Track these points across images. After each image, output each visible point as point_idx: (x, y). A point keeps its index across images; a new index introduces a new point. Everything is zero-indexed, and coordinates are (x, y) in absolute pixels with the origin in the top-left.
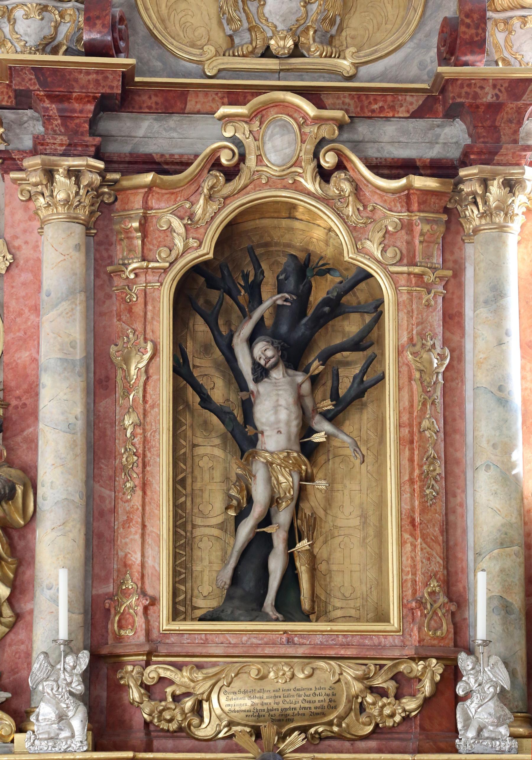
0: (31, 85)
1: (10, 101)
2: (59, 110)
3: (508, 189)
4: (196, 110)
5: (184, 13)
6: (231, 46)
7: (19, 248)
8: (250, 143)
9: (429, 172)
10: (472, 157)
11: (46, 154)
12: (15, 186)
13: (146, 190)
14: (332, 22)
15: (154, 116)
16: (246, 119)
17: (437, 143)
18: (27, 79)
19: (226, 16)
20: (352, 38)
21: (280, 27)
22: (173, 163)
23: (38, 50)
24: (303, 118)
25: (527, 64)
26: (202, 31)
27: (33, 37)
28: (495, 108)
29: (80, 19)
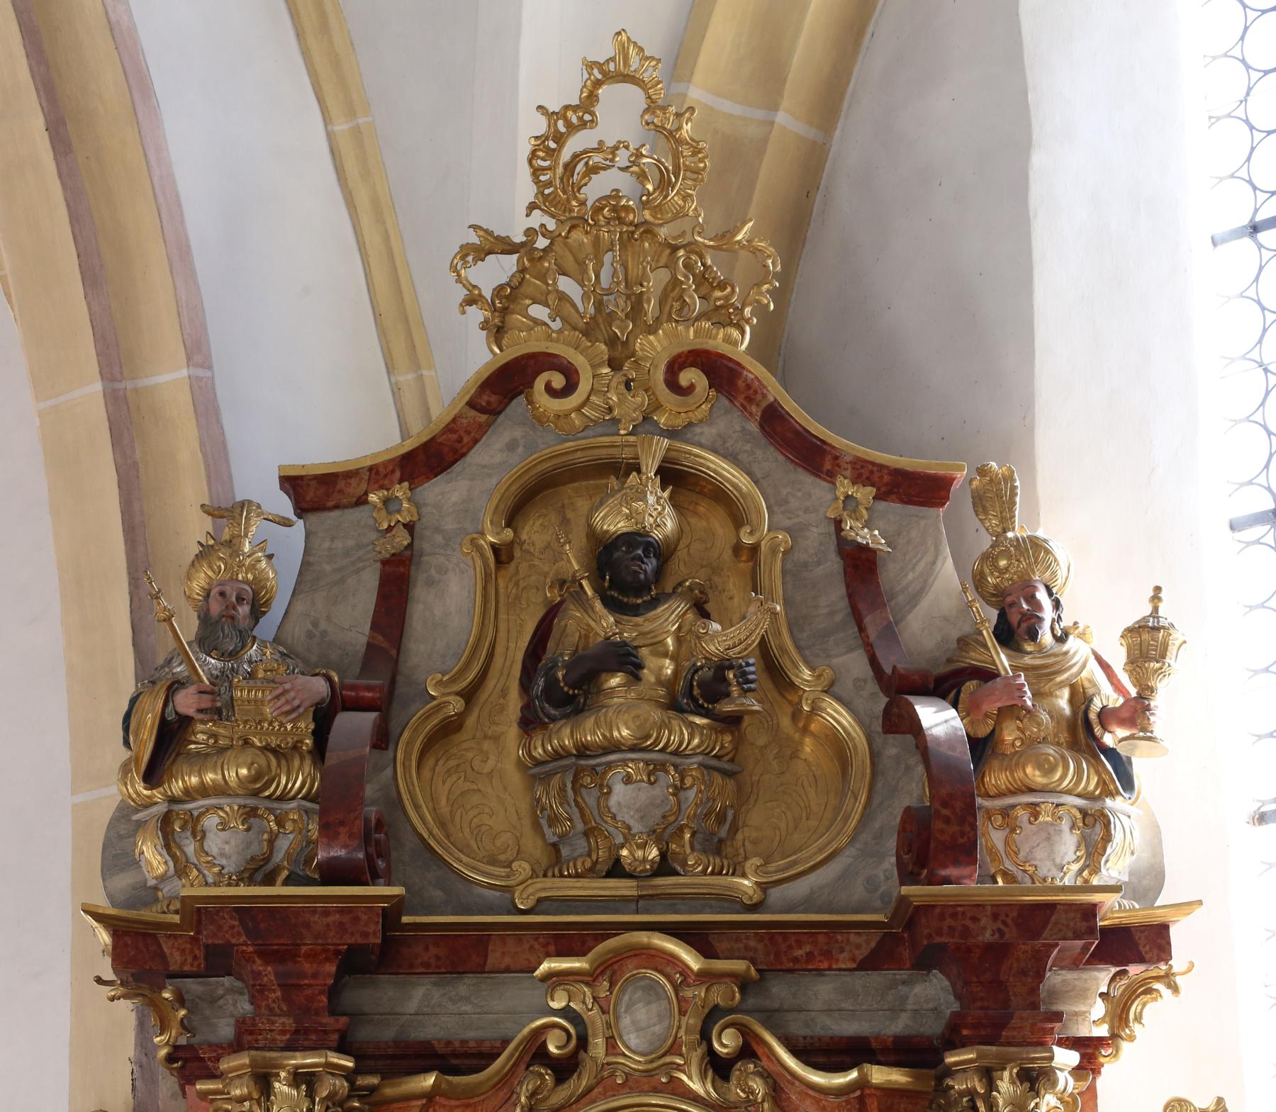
0: (233, 936)
1: (196, 963)
2: (276, 974)
3: (1027, 1085)
4: (503, 966)
5: (476, 811)
6: (555, 862)
8: (593, 1016)
9: (892, 1058)
10: (965, 1032)
11: (257, 1049)
12: (204, 1104)
13: (424, 1101)
14: (721, 818)
15: (434, 978)
16: (586, 979)
17: (902, 1010)
18: (226, 928)
19: (546, 813)
21: (637, 827)
22: (467, 1055)
23: (242, 880)
24: (681, 974)
25: (1044, 880)
26: (506, 838)
27: (234, 858)
28: (998, 952)
29: (310, 827)
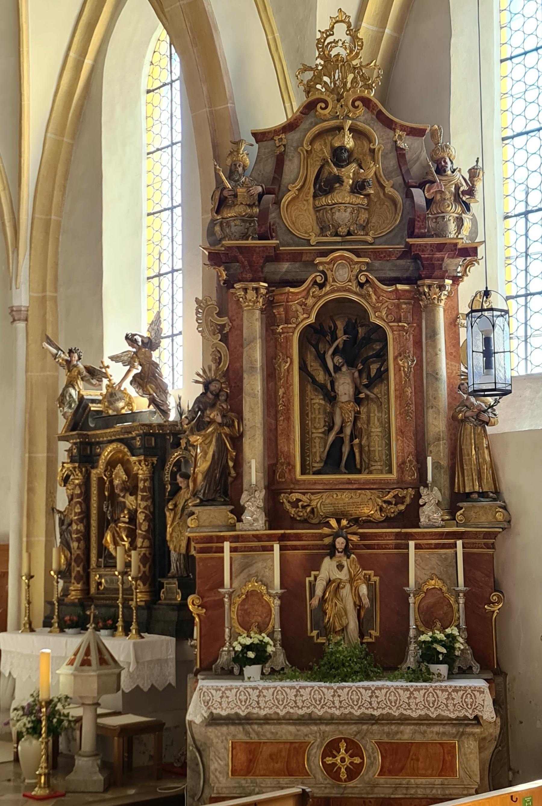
7: (234, 320)
20: (373, 227)
